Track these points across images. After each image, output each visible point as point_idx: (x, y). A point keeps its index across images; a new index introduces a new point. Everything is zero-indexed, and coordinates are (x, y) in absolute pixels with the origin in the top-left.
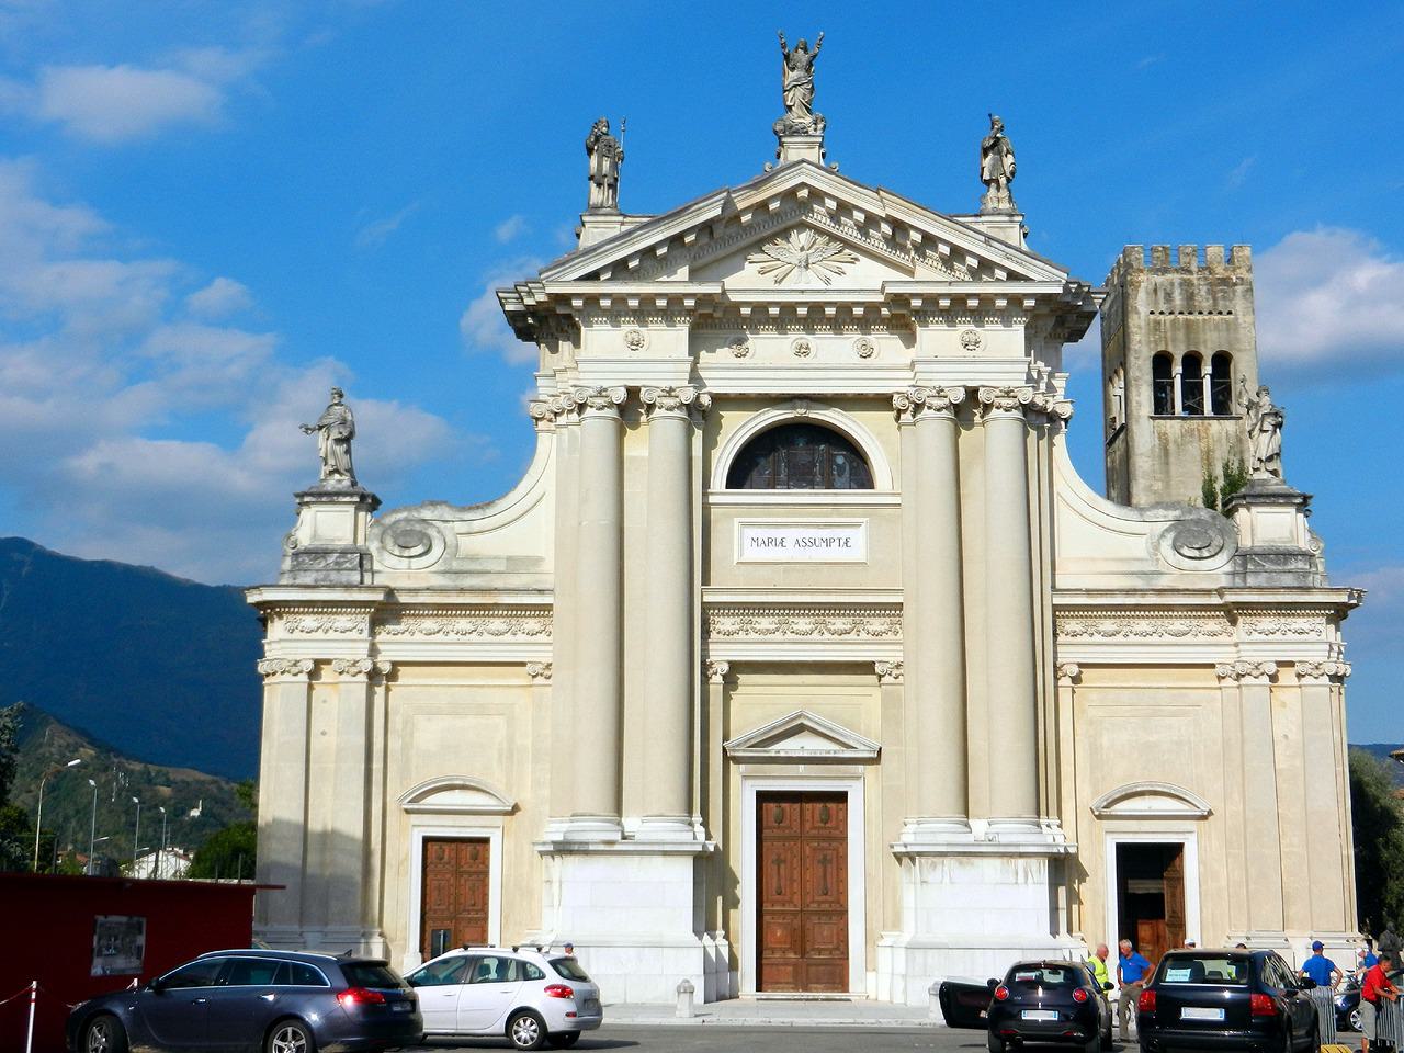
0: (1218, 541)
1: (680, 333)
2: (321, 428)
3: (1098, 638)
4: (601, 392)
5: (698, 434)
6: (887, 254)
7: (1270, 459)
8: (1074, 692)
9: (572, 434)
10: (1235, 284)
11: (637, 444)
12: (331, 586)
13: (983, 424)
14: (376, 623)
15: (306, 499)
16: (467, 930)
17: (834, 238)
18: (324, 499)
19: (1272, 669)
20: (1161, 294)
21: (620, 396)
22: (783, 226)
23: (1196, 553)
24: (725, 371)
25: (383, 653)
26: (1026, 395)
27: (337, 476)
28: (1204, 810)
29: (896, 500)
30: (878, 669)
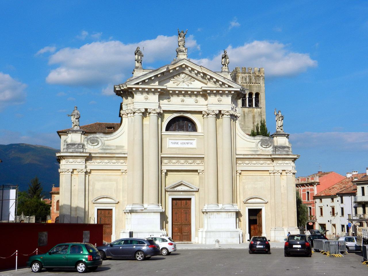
0: (270, 144)
1: (156, 96)
2: (72, 115)
3: (245, 165)
4: (139, 110)
5: (160, 119)
6: (196, 77)
7: (281, 126)
8: (240, 176)
9: (131, 119)
10: (261, 77)
11: (146, 121)
12: (77, 152)
13: (222, 118)
14: (86, 160)
15: (70, 132)
16: (107, 229)
17: (190, 76)
18: (74, 132)
19: (281, 172)
20: (244, 79)
21: (143, 110)
22: (178, 73)
23: (265, 147)
24: (166, 105)
25: (88, 167)
26: (232, 112)
27: (76, 127)
29: (203, 134)
30: (199, 171)
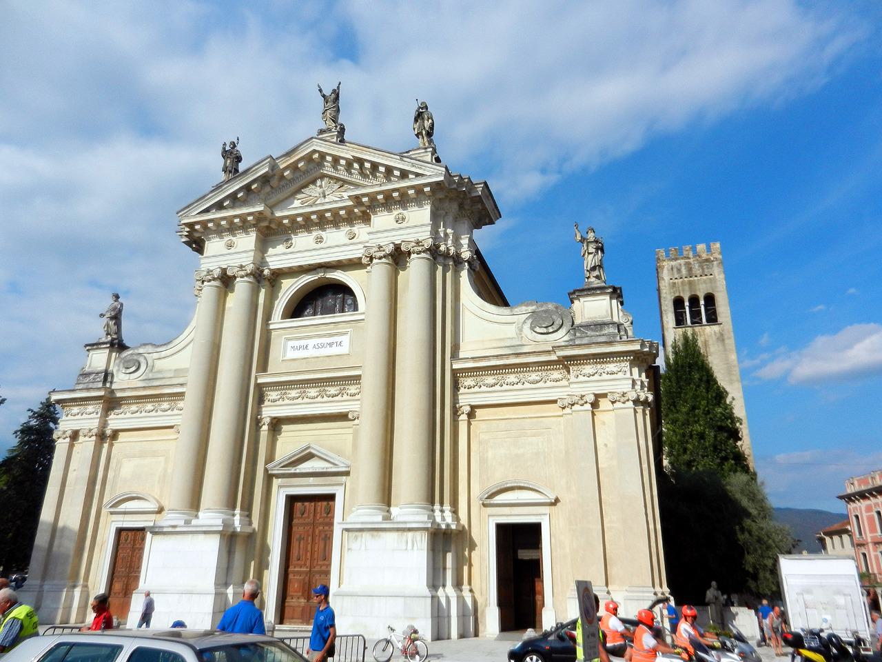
10: (713, 261)
18: (95, 347)
20: (675, 270)
23: (545, 330)
24: (278, 258)
28: (552, 498)
30: (350, 416)
